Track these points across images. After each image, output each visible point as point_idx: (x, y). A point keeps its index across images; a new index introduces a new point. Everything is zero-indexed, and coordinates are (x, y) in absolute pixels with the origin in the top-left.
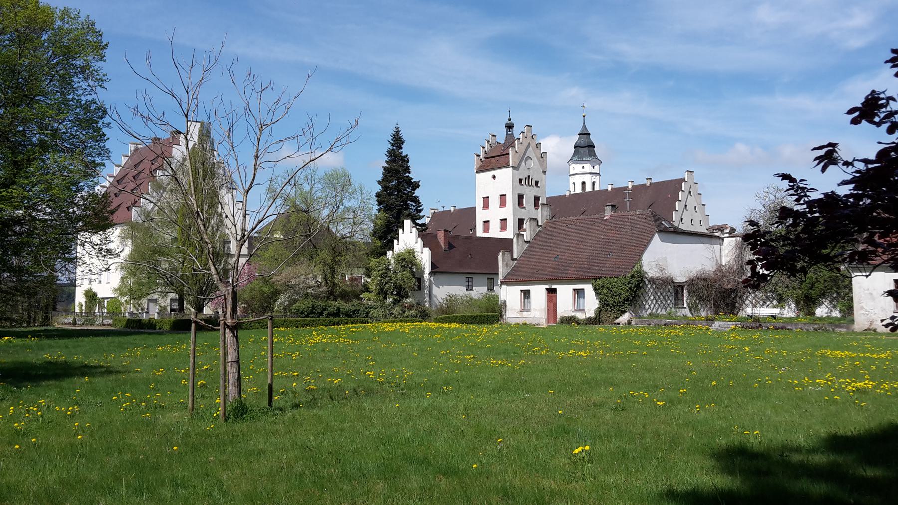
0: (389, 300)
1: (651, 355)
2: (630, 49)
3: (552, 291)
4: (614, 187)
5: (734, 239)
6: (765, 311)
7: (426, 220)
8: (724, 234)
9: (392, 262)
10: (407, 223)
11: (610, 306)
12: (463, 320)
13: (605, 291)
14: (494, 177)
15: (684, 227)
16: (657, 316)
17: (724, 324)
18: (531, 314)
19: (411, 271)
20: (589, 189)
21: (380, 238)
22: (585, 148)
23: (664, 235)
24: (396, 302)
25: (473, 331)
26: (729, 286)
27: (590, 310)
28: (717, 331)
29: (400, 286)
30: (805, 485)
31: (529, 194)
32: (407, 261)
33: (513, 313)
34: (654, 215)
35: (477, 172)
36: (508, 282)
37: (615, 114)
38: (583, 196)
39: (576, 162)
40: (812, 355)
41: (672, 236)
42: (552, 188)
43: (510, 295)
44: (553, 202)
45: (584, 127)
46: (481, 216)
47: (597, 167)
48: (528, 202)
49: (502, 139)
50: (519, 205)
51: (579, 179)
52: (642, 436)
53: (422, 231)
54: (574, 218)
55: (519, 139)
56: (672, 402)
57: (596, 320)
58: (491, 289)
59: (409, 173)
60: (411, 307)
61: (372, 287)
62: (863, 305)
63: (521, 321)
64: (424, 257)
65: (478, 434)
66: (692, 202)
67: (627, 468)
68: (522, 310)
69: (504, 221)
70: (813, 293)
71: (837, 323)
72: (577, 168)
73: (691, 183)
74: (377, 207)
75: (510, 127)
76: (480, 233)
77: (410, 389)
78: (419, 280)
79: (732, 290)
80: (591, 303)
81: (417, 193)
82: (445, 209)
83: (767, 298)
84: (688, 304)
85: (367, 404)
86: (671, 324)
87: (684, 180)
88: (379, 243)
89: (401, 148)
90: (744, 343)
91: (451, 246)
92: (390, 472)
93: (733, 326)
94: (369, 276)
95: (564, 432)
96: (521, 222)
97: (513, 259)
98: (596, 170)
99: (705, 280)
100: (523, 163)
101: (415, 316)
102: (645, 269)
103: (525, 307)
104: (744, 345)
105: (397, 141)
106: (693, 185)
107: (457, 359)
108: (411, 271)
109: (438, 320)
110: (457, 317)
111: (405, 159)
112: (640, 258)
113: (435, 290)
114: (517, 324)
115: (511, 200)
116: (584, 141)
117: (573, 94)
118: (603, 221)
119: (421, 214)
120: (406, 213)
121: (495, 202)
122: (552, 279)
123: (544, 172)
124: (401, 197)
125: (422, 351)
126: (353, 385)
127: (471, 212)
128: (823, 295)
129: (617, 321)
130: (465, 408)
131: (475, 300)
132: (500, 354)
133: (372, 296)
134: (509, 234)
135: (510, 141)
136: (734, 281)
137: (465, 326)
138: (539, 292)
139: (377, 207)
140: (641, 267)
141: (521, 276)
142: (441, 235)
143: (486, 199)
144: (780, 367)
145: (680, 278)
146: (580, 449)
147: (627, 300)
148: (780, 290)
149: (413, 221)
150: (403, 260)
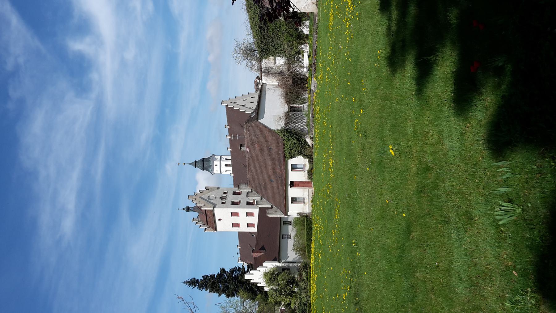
0: (296, 290)
1: (332, 122)
2: (145, 133)
3: (292, 184)
4: (228, 135)
5: (263, 77)
6: (306, 61)
7: (245, 265)
8: (260, 83)
9: (271, 287)
10: (247, 276)
11: (301, 149)
12: (309, 240)
13: (292, 152)
14: (220, 220)
15: (254, 106)
16: (308, 122)
17: (313, 84)
18: (306, 197)
19: (278, 275)
20: (230, 162)
21: (256, 295)
22: (205, 164)
23: (260, 116)
24: (297, 285)
25: (317, 233)
26: (291, 81)
27: (304, 161)
28: (317, 88)
29: (287, 282)
30: (410, 20)
31: (231, 198)
32: (271, 277)
33: (306, 209)
34: (247, 122)
35: (216, 230)
36: (285, 211)
37: (184, 144)
38: (233, 166)
39: (213, 169)
40: (332, 33)
41: (260, 112)
42: (228, 184)
43: (294, 210)
44: (237, 184)
45: (191, 164)
46: (244, 229)
47: (216, 157)
48: (236, 199)
49: (196, 214)
50: (238, 204)
51: (223, 168)
52: (382, 118)
53: (252, 267)
54: (247, 169)
55: (196, 204)
56: (361, 105)
57: (310, 158)
58: (290, 223)
59: (214, 275)
60: (301, 275)
61: (288, 301)
62: (303, 7)
63: (311, 204)
64: (269, 266)
65: (383, 217)
66: (240, 102)
67: (403, 122)
68: (304, 203)
69: (247, 214)
70: (295, 34)
71: (313, 22)
72: (216, 169)
73: (229, 103)
74: (236, 297)
75: (188, 209)
76: (255, 230)
77: (354, 268)
78: (283, 269)
79: (293, 79)
80: (300, 160)
81: (227, 270)
82: (239, 253)
83: (298, 60)
84: (301, 104)
85: (365, 295)
86: (313, 114)
87: (227, 106)
88: (259, 296)
89: (198, 280)
90: (325, 71)
91: (263, 248)
92: (409, 270)
93: (315, 79)
94: (280, 303)
95: (380, 164)
96: (249, 204)
97: (272, 207)
98: (218, 157)
99: (287, 94)
100: (212, 201)
101: (307, 272)
102: (279, 128)
103: (302, 201)
104: (326, 71)
105: (193, 282)
106: (229, 101)
107: (334, 241)
108: (278, 275)
109: (310, 256)
110: (307, 244)
111: (205, 278)
112: (274, 131)
113: (290, 259)
114: (312, 206)
115: (235, 210)
116: (200, 165)
117: (170, 168)
118: (250, 152)
119: (241, 267)
120: (240, 277)
121: (235, 220)
122: (284, 183)
123: (218, 188)
124: (230, 280)
125: (329, 264)
126: (352, 306)
127: (242, 235)
128: (297, 30)
129: (311, 145)
130: (366, 229)
131: (297, 233)
132: (331, 214)
133: (293, 301)
134: (256, 211)
135: (197, 209)
136: (287, 78)
137: (313, 238)
138: (293, 192)
139: (236, 297)
140: (278, 130)
141: (283, 203)
142: (255, 255)
143: (234, 225)
144: (339, 48)
145: (286, 108)
146: (391, 151)
147: (298, 139)
148: (293, 53)
149: (245, 273)
150: (270, 279)
